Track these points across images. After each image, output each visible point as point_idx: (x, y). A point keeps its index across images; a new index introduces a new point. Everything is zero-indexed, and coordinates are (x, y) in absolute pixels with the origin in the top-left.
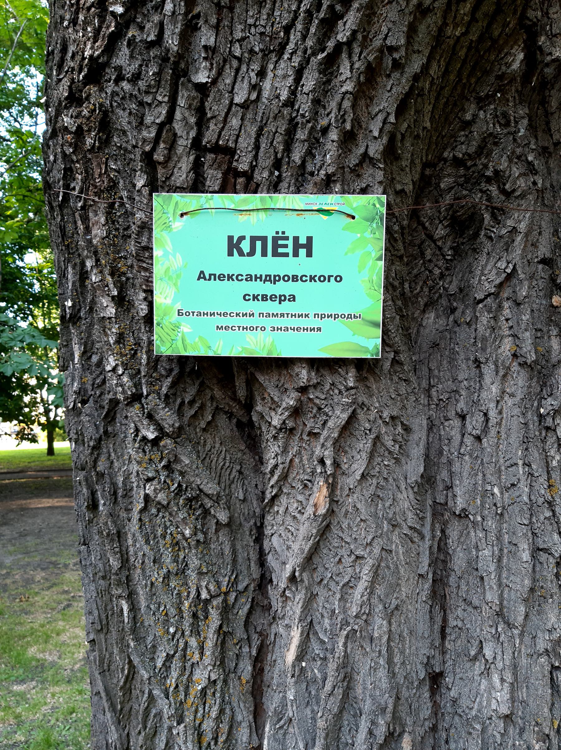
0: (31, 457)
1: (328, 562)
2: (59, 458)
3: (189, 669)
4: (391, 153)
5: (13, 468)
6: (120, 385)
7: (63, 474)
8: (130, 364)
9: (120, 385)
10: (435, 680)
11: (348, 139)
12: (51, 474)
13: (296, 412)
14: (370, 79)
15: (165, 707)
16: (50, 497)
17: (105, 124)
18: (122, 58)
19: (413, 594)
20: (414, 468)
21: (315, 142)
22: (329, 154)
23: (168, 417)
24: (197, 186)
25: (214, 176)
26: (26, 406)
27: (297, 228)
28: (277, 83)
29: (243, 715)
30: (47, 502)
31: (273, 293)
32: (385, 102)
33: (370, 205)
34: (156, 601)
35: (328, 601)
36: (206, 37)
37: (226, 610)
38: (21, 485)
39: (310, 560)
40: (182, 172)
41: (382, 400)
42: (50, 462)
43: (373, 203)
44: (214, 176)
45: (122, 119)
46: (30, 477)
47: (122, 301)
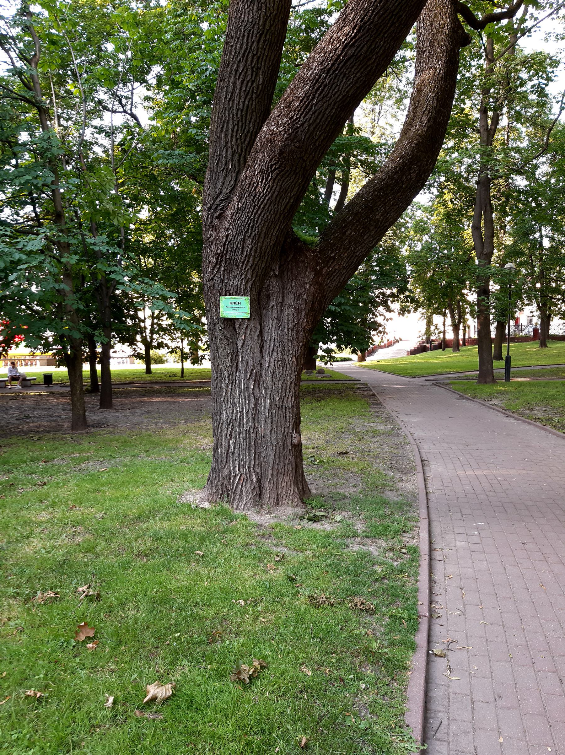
1: (245, 346)
2: (157, 376)
3: (226, 363)
4: (251, 290)
5: (122, 381)
6: (216, 321)
9: (216, 321)
10: (261, 364)
11: (245, 290)
12: (153, 385)
13: (240, 325)
14: (247, 282)
15: (223, 369)
18: (215, 278)
19: (257, 351)
20: (257, 333)
21: (241, 289)
22: (242, 291)
23: (223, 326)
24: (226, 295)
25: (228, 294)
26: (560, 270)
27: (238, 301)
28: (236, 282)
29: (235, 370)
30: (155, 399)
31: (236, 309)
32: (249, 285)
33: (248, 298)
35: (245, 352)
36: (226, 277)
37: (232, 355)
38: (134, 391)
39: (242, 346)
40: (224, 293)
41: (252, 324)
42: (148, 378)
43: (248, 298)
44: (228, 294)
45: (216, 286)
46: (137, 387)
47: (216, 310)
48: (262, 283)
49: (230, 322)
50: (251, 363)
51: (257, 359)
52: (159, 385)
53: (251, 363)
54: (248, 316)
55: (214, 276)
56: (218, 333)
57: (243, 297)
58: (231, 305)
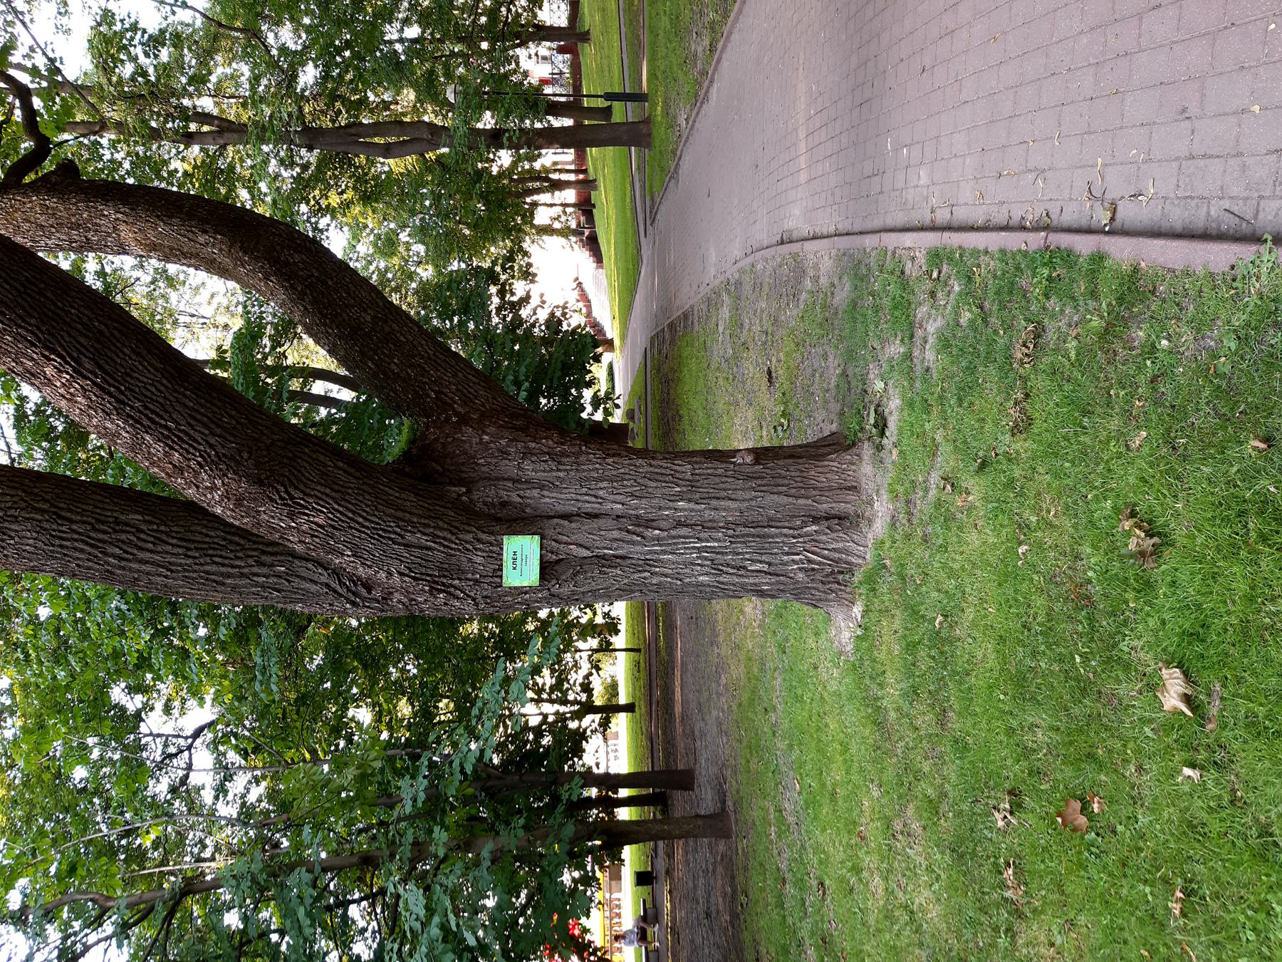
0: (636, 732)
1: (588, 545)
2: (638, 694)
3: (617, 575)
4: (492, 533)
6: (545, 593)
7: (654, 684)
8: (540, 591)
9: (545, 593)
11: (492, 544)
14: (479, 540)
15: (626, 581)
16: (673, 693)
17: (486, 597)
19: (595, 524)
20: (566, 523)
21: (491, 551)
23: (554, 582)
24: (501, 577)
26: (458, 8)
27: (511, 555)
29: (629, 561)
30: (678, 696)
32: (484, 536)
34: (601, 583)
35: (598, 544)
36: (470, 576)
38: (664, 733)
39: (587, 548)
40: (498, 580)
41: (550, 532)
42: (641, 708)
43: (505, 538)
49: (547, 569)
51: (610, 523)
53: (616, 534)
54: (537, 538)
58: (519, 568)
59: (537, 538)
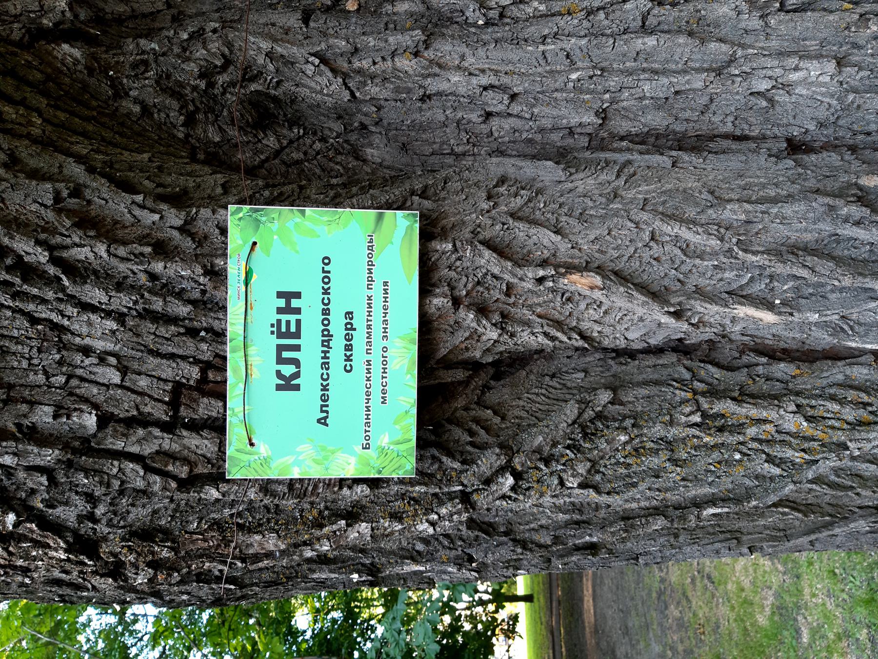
1: (657, 273)
2: (536, 588)
3: (783, 437)
4: (179, 200)
5: (548, 643)
6: (450, 517)
7: (554, 584)
9: (450, 517)
10: (796, 147)
12: (554, 598)
14: (92, 224)
15: (828, 465)
16: (581, 600)
18: (68, 514)
19: (695, 173)
20: (548, 172)
21: (166, 289)
23: (489, 461)
24: (218, 427)
25: (206, 408)
26: (475, 627)
27: (267, 309)
28: (98, 333)
29: (837, 372)
30: (588, 603)
31: (344, 338)
32: (118, 205)
35: (703, 273)
36: (43, 416)
37: (714, 393)
40: (201, 444)
41: (468, 210)
42: (541, 600)
43: (238, 221)
44: (206, 408)
45: (139, 514)
46: (558, 623)
47: (353, 516)
48: (140, 131)
49: (455, 394)
50: (801, 221)
51: (762, 169)
52: (554, 589)
53: (801, 221)
54: (401, 228)
55: (46, 524)
56: (542, 505)
57: (235, 270)
58: (310, 378)
59: (401, 228)
